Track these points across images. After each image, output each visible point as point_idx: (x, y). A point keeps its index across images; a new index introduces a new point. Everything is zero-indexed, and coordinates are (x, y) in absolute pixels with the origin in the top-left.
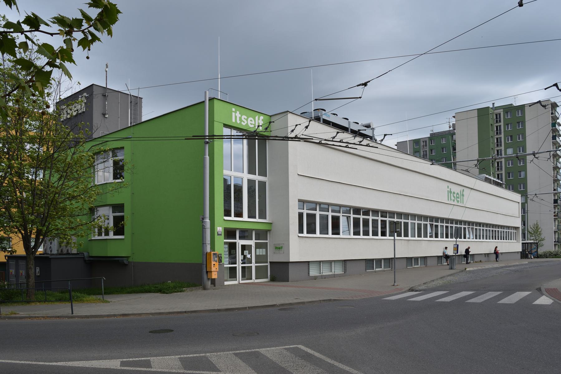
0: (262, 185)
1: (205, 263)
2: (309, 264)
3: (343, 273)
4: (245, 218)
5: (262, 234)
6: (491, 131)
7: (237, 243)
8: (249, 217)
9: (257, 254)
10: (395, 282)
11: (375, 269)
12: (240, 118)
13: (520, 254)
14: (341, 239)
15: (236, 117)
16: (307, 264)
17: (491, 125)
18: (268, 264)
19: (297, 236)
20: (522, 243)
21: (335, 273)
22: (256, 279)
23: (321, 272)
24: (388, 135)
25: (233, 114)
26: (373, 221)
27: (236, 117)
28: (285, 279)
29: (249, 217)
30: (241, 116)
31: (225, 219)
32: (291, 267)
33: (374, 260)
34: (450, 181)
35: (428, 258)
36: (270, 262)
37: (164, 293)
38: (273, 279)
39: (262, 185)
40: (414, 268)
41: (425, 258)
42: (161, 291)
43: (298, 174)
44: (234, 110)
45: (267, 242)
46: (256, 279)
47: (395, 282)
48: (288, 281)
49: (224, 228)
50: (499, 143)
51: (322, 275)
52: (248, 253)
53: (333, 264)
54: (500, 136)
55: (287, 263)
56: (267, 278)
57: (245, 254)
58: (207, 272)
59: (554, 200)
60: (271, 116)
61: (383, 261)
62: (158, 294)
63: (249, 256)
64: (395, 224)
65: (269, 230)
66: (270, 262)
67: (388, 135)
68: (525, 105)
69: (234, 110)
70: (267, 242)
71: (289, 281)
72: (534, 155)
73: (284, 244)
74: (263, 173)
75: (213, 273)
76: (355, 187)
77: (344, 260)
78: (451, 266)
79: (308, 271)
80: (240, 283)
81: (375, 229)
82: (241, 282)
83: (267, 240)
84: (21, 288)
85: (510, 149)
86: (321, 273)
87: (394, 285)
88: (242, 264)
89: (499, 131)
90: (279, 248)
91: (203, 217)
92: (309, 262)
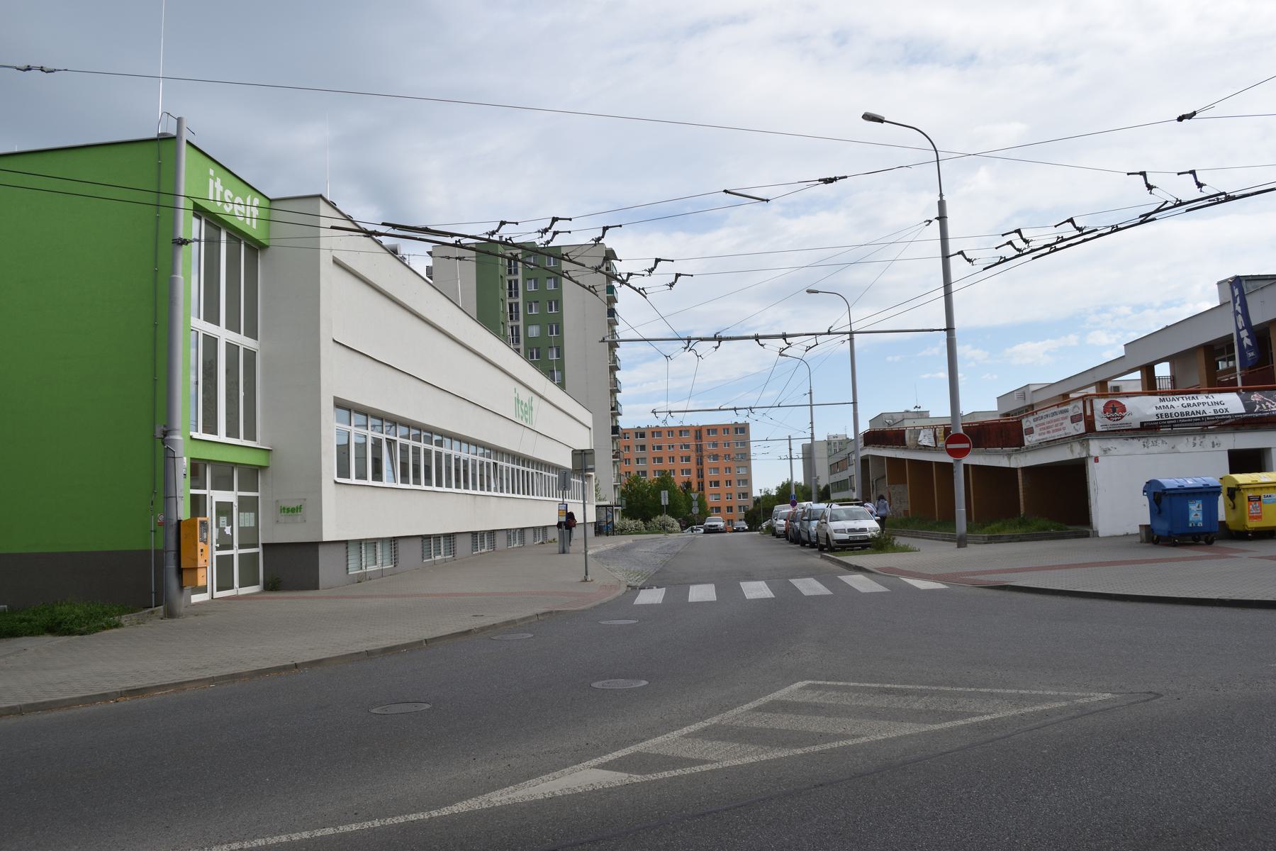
0: (250, 355)
1: (172, 546)
2: (347, 548)
3: (393, 566)
4: (222, 437)
5: (251, 475)
6: (500, 290)
7: (207, 496)
8: (228, 435)
9: (241, 525)
10: (587, 574)
11: (433, 557)
12: (222, 194)
13: (593, 525)
14: (394, 490)
15: (215, 189)
16: (344, 546)
17: (501, 277)
18: (260, 550)
19: (333, 482)
20: (597, 506)
21: (384, 568)
22: (240, 587)
23: (364, 564)
24: (683, 275)
25: (211, 181)
26: (415, 455)
27: (215, 189)
28: (309, 581)
29: (228, 435)
30: (224, 190)
31: (194, 437)
32: (322, 551)
33: (430, 538)
34: (521, 378)
35: (497, 533)
36: (264, 545)
37: (70, 633)
38: (272, 585)
39: (247, 362)
40: (481, 553)
41: (450, 537)
42: (56, 628)
43: (334, 340)
44: (212, 172)
45: (258, 497)
46: (240, 587)
47: (587, 574)
48: (317, 588)
49: (191, 459)
50: (514, 314)
51: (366, 573)
52: (225, 523)
53: (379, 545)
54: (516, 301)
55: (312, 548)
56: (256, 583)
57: (221, 526)
58: (180, 571)
59: (612, 427)
60: (271, 201)
61: (442, 539)
62: (48, 641)
63: (228, 530)
64: (585, 454)
65: (263, 468)
66: (264, 545)
67: (683, 275)
68: (560, 246)
69: (212, 172)
70: (258, 497)
71: (320, 587)
72: (757, 340)
73: (305, 499)
74: (252, 332)
75: (199, 570)
76: (408, 377)
77: (394, 538)
78: (564, 548)
79: (345, 563)
80: (214, 597)
81: (465, 469)
82: (218, 595)
83: (257, 491)
84: (595, 556)
85: (534, 327)
86: (364, 568)
87: (586, 580)
88: (218, 549)
89: (513, 291)
90: (293, 510)
91: (165, 429)
92: (346, 542)
